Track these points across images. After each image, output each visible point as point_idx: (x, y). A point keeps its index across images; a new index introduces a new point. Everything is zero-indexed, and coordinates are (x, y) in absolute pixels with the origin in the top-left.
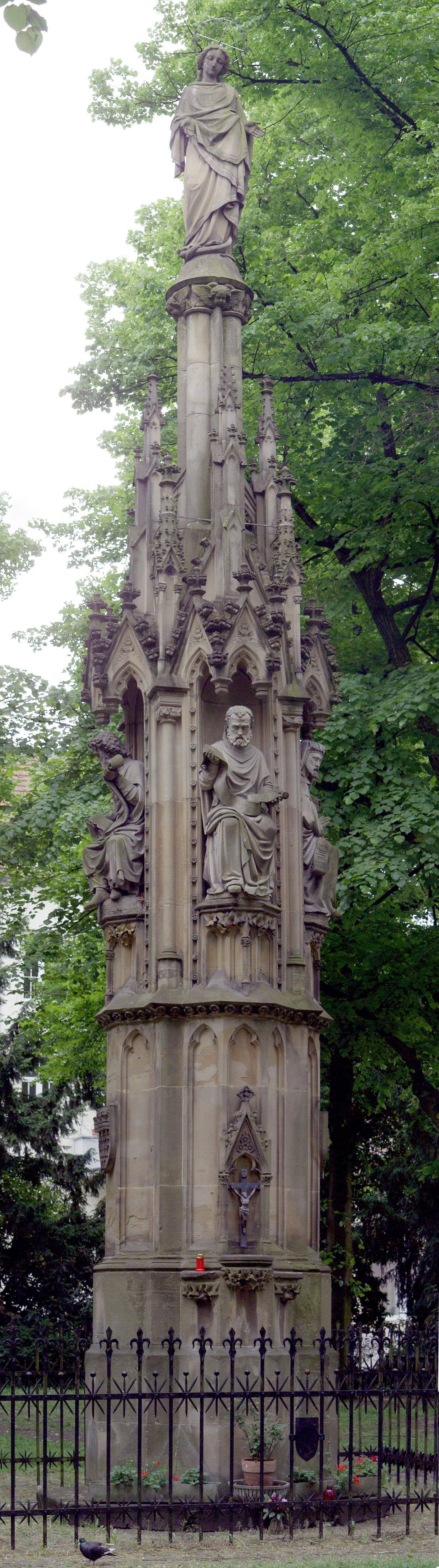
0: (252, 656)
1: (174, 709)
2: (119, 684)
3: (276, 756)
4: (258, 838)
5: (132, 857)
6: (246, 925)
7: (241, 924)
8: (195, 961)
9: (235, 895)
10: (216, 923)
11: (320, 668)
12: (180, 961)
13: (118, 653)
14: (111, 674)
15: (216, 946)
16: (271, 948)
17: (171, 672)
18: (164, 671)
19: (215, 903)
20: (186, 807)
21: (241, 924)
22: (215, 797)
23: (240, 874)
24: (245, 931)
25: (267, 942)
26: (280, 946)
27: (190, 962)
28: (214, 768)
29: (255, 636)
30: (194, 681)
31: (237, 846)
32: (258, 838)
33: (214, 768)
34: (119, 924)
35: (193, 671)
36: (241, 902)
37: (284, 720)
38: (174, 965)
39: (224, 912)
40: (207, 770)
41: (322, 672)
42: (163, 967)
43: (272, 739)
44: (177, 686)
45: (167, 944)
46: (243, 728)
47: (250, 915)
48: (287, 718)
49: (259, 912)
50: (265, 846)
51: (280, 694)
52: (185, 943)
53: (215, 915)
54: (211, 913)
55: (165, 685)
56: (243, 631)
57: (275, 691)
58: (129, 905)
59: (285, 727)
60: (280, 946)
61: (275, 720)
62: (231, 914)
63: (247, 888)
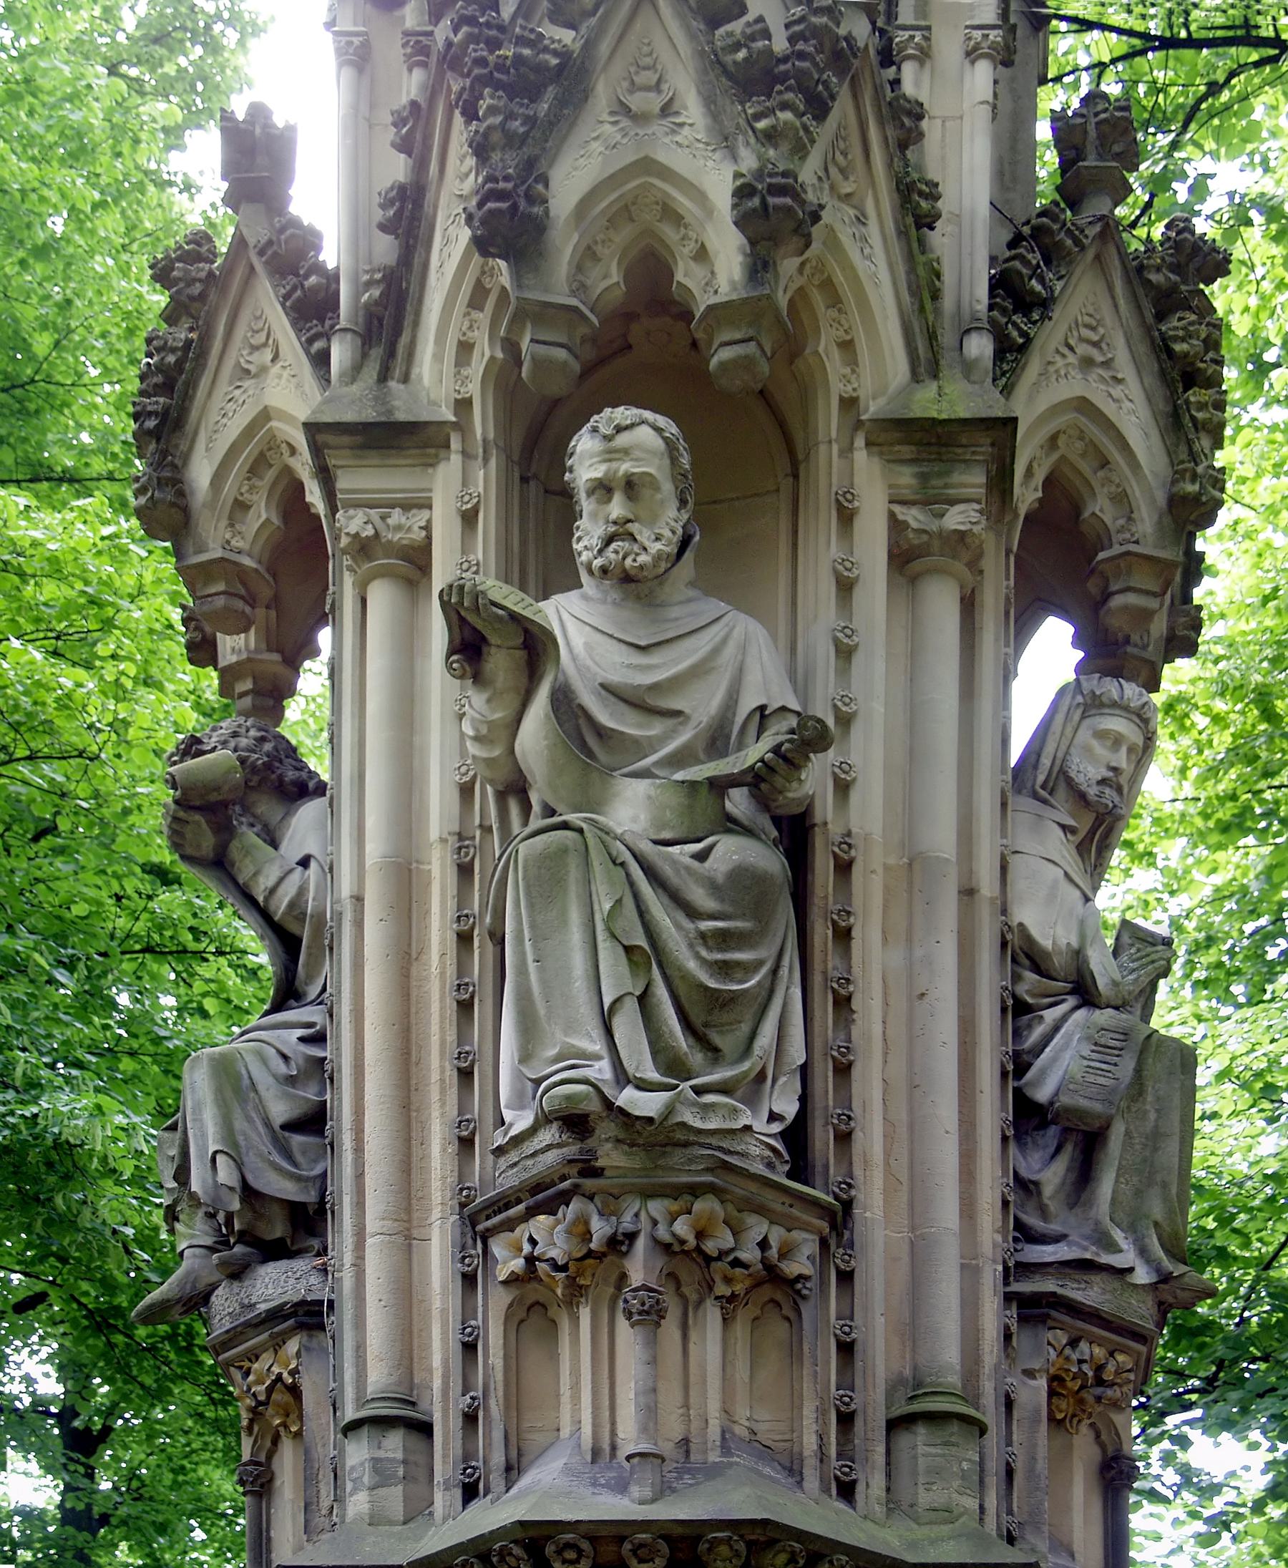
0: (683, 202)
1: (396, 516)
2: (241, 507)
3: (845, 653)
4: (693, 913)
5: (280, 1111)
6: (641, 1243)
7: (619, 1244)
8: (470, 1419)
9: (575, 1122)
10: (531, 1260)
11: (1125, 368)
12: (424, 1429)
13: (223, 387)
14: (201, 472)
15: (554, 1357)
16: (794, 1353)
17: (384, 377)
18: (355, 371)
19: (510, 1180)
20: (439, 869)
21: (619, 1244)
22: (534, 798)
23: (598, 1046)
24: (640, 1268)
25: (779, 1330)
26: (846, 1349)
27: (456, 1422)
28: (500, 662)
29: (693, 110)
30: (473, 389)
31: (576, 936)
32: (693, 913)
33: (500, 662)
34: (254, 1356)
35: (465, 348)
36: (611, 1157)
37: (896, 525)
38: (394, 1443)
39: (549, 1207)
40: (478, 678)
41: (1133, 387)
42: (358, 1453)
43: (828, 588)
44: (401, 416)
45: (378, 1376)
46: (631, 486)
47: (656, 1207)
48: (913, 517)
49: (695, 1191)
50: (724, 939)
51: (873, 408)
52: (437, 1361)
53: (523, 1231)
54: (510, 1225)
55: (349, 416)
56: (636, 102)
57: (849, 404)
58: (275, 1283)
59: (906, 559)
60: (846, 1349)
61: (847, 517)
62: (575, 1206)
63: (628, 1098)
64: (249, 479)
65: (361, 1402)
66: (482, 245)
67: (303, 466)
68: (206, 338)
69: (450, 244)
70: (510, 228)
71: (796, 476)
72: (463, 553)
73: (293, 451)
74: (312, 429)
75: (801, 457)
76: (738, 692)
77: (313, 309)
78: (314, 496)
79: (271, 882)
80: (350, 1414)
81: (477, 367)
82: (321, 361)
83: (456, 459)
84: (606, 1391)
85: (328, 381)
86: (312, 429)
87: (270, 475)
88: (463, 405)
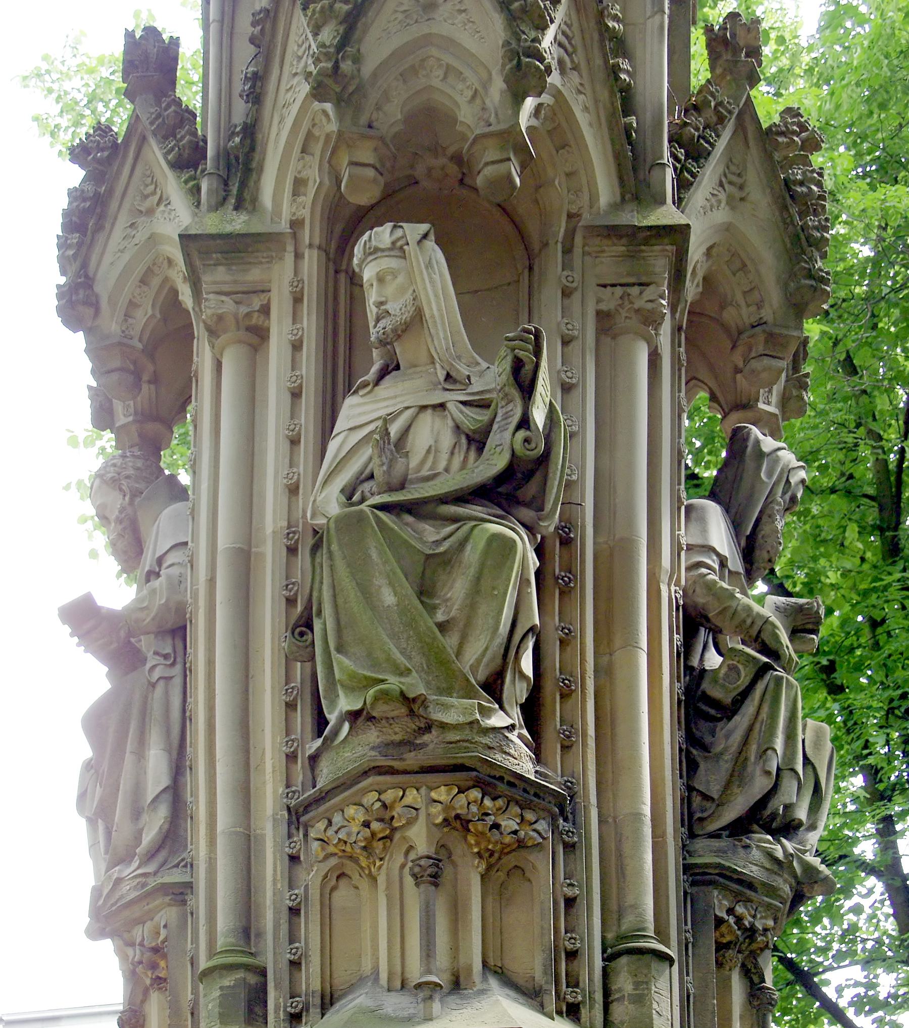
30: (305, 213)
64: (140, 287)
65: (211, 954)
66: (319, 92)
67: (178, 275)
68: (110, 192)
69: (291, 94)
70: (334, 83)
71: (531, 268)
72: (293, 370)
73: (170, 262)
74: (186, 239)
75: (536, 246)
76: (257, 968)
77: (188, 161)
78: (186, 297)
79: (329, 990)
80: (203, 964)
81: (307, 199)
82: (196, 190)
83: (289, 258)
84: (398, 946)
85: (199, 203)
86: (186, 239)
87: (156, 282)
88: (297, 224)
